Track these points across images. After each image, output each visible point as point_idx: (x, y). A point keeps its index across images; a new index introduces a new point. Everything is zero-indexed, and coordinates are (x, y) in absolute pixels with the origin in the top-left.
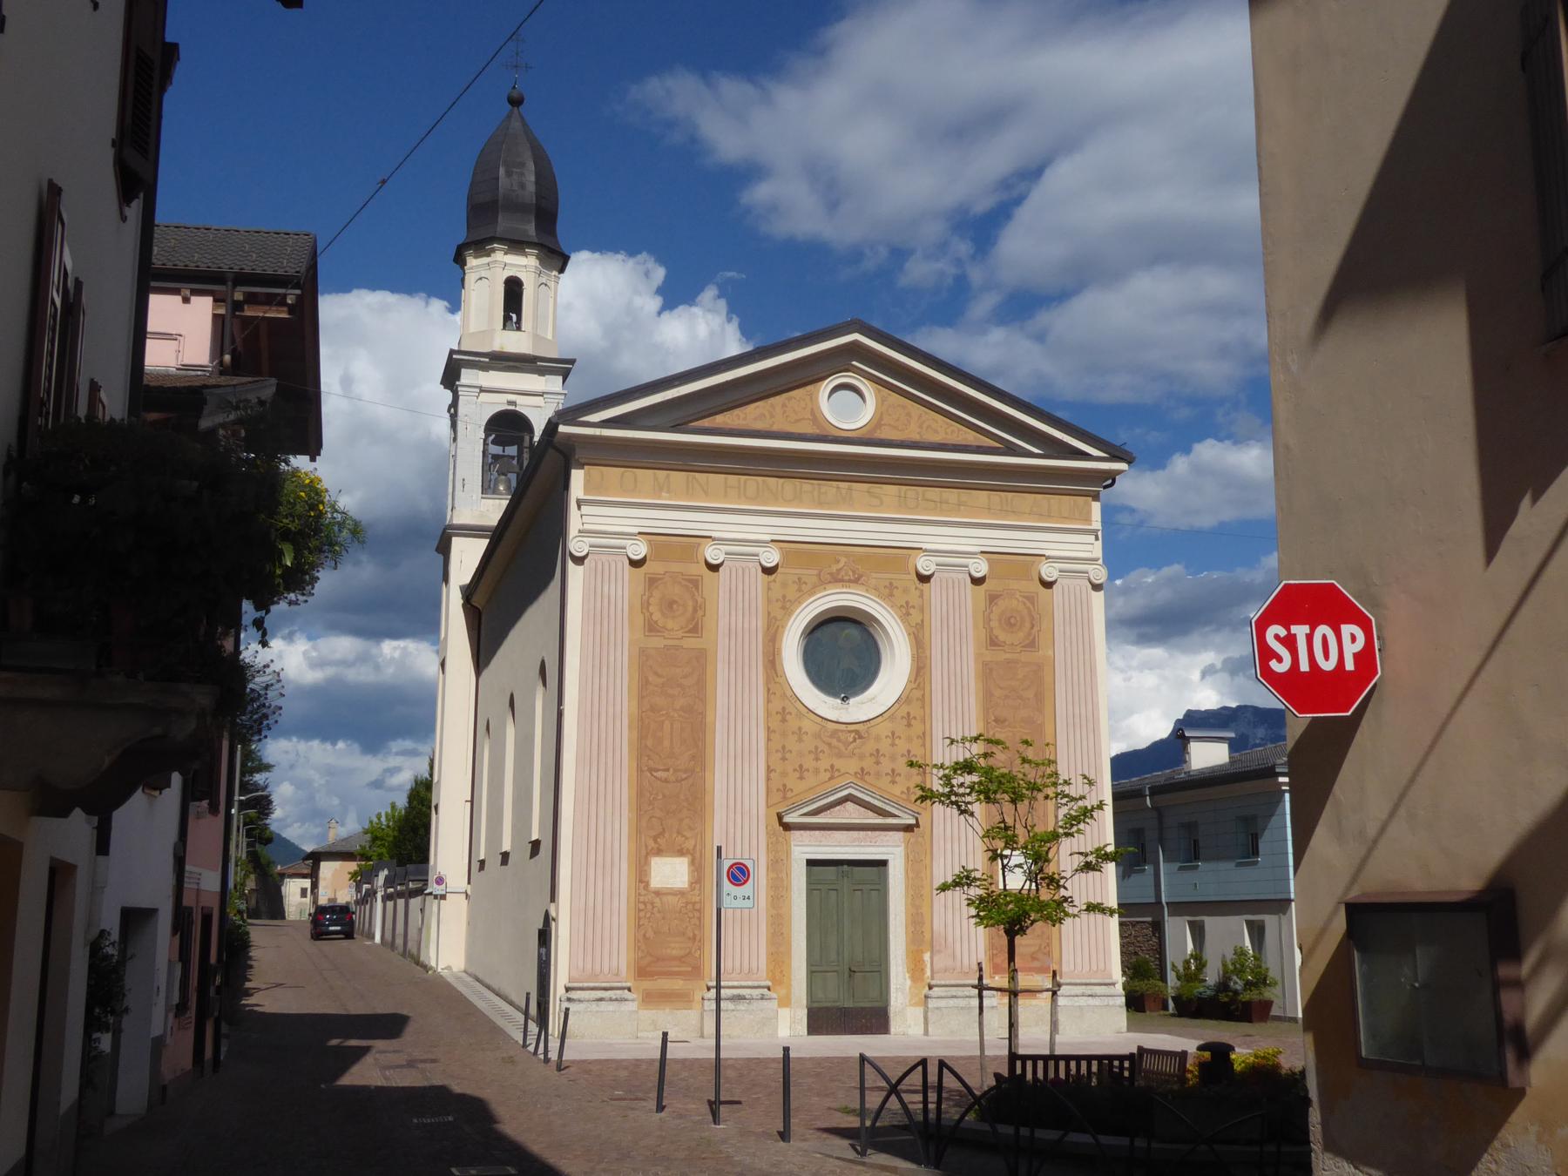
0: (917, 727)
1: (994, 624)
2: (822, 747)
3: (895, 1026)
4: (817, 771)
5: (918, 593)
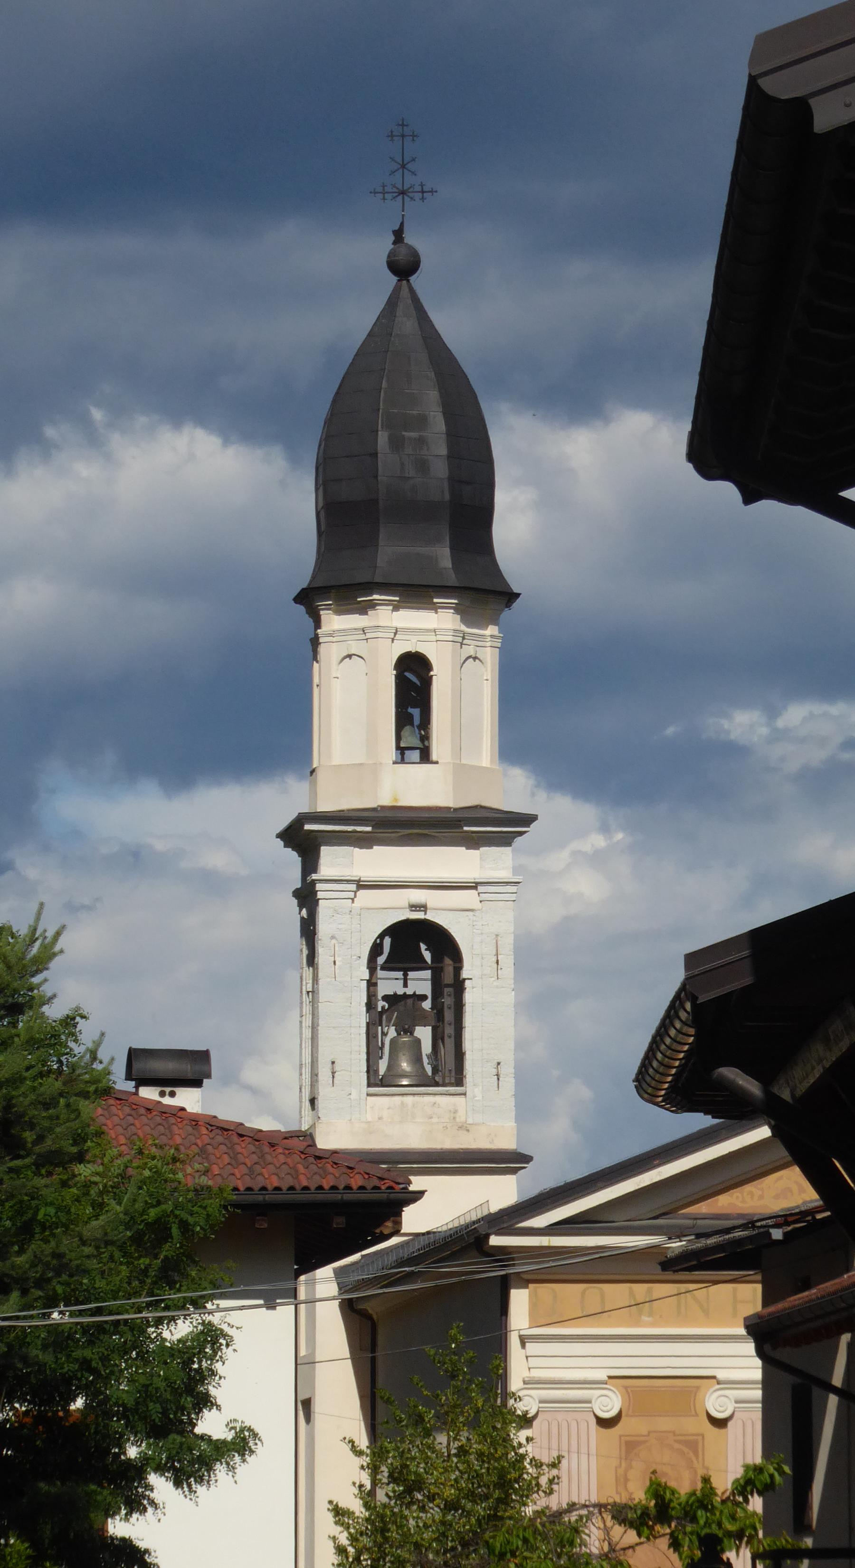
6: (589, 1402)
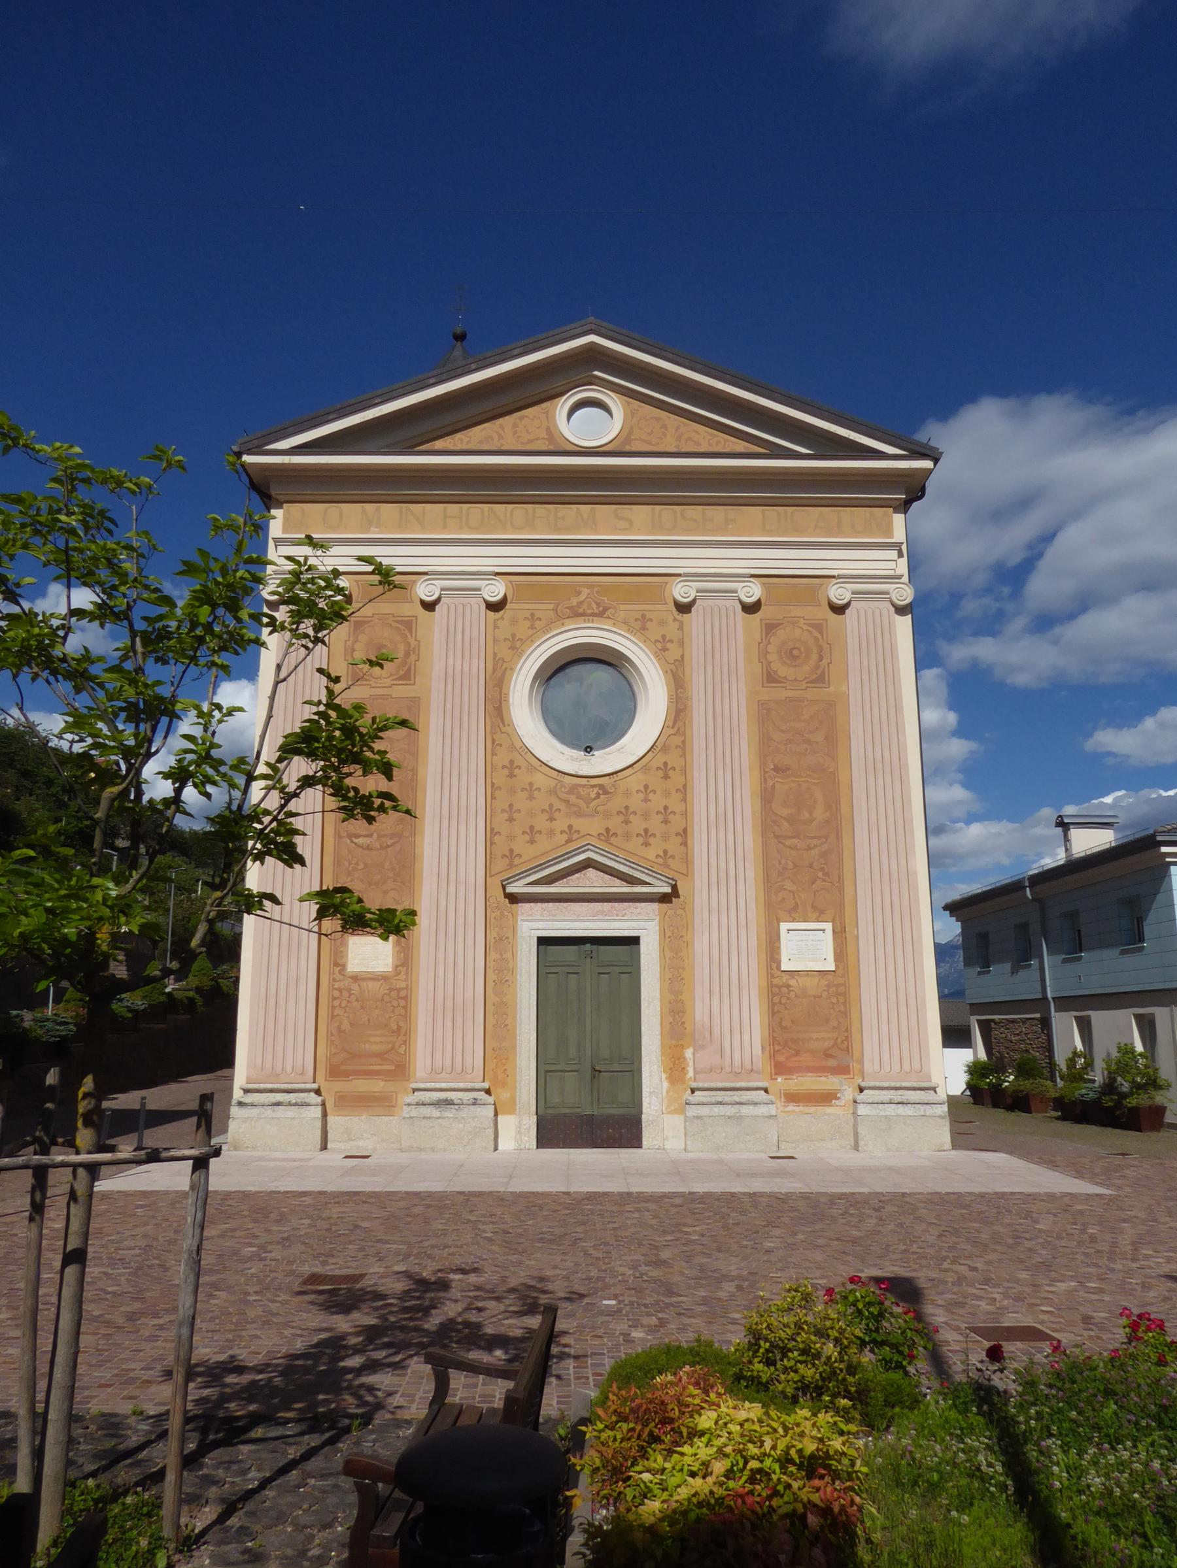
0: (676, 778)
1: (773, 657)
2: (557, 804)
3: (649, 1137)
4: (551, 833)
5: (677, 625)
6: (479, 590)
